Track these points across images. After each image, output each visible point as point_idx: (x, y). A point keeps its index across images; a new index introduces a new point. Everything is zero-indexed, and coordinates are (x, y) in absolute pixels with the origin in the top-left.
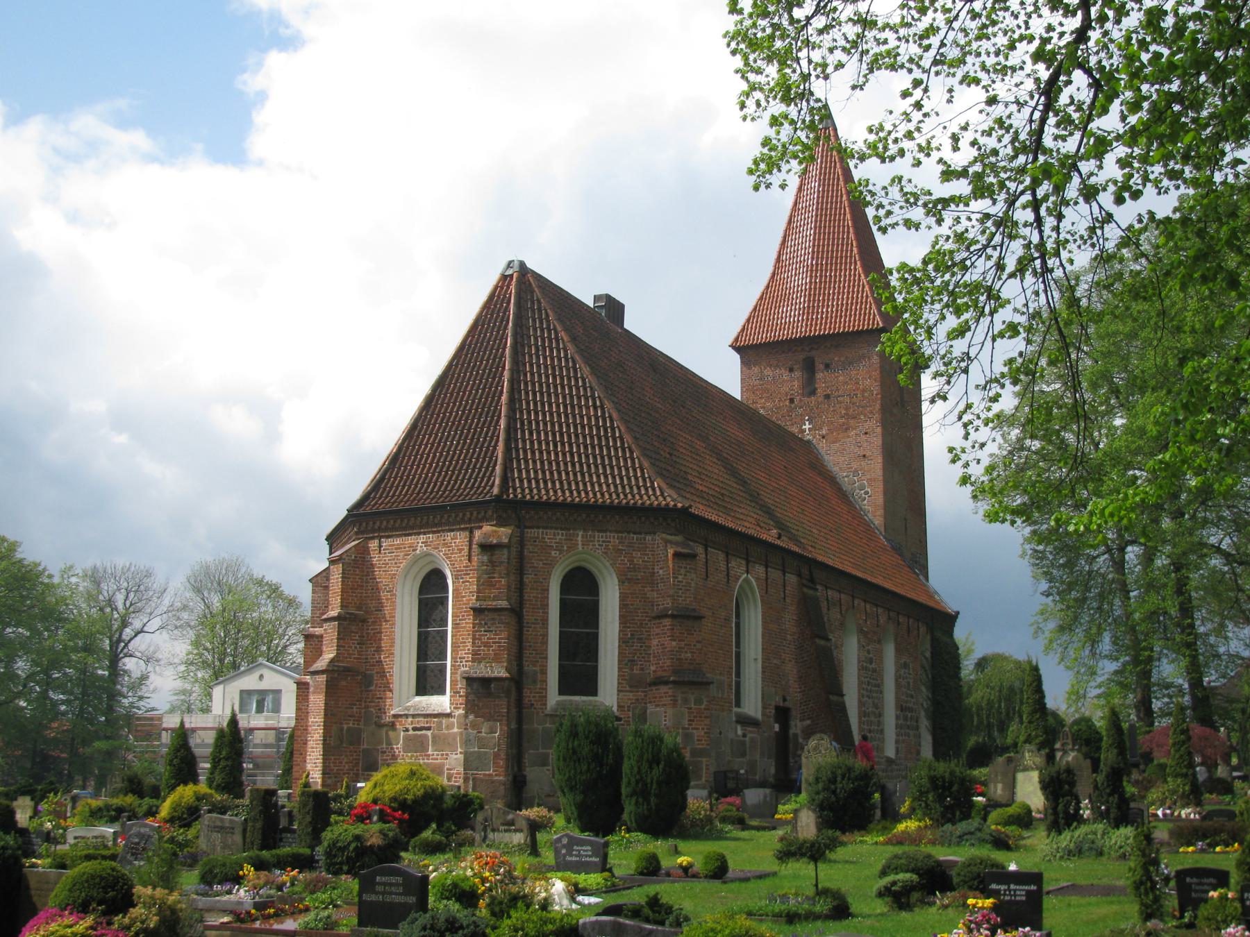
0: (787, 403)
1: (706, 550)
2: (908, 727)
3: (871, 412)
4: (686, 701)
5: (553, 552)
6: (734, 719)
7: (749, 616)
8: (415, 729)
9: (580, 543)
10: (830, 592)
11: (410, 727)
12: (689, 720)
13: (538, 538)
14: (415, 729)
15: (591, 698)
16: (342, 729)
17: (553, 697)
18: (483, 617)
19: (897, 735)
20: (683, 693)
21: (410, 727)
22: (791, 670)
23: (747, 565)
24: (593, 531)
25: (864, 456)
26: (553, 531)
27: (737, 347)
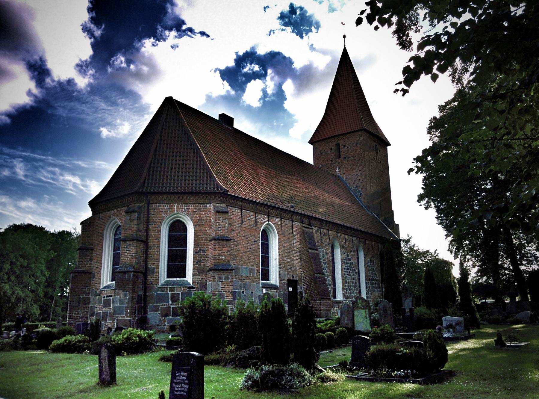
0: (330, 162)
1: (241, 211)
2: (374, 288)
3: (362, 162)
4: (220, 278)
5: (163, 214)
6: (261, 286)
7: (272, 241)
8: (107, 296)
9: (176, 209)
10: (322, 230)
11: (105, 296)
12: (222, 287)
13: (156, 208)
14: (107, 296)
15: (268, 282)
16: (80, 298)
17: (163, 278)
18: (126, 244)
19: (367, 291)
20: (218, 275)
21: (105, 296)
22: (297, 263)
23: (268, 218)
24: (182, 204)
25: (360, 180)
26: (163, 205)
27: (311, 142)
